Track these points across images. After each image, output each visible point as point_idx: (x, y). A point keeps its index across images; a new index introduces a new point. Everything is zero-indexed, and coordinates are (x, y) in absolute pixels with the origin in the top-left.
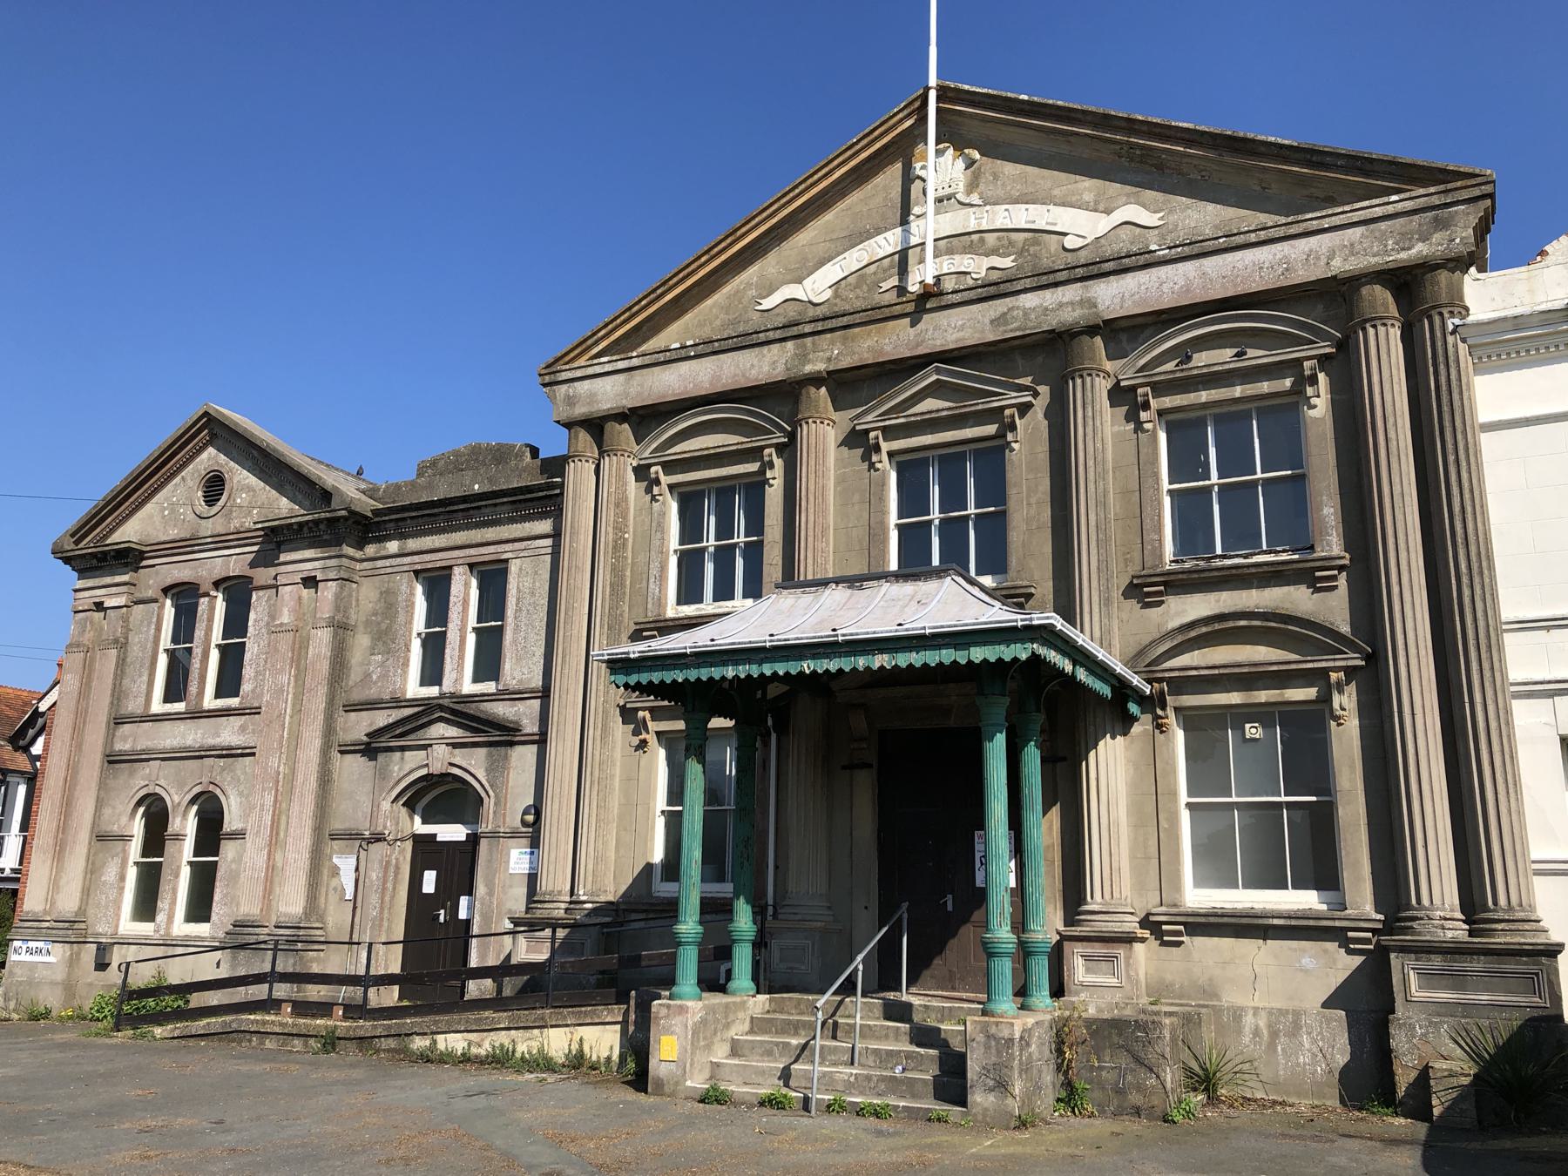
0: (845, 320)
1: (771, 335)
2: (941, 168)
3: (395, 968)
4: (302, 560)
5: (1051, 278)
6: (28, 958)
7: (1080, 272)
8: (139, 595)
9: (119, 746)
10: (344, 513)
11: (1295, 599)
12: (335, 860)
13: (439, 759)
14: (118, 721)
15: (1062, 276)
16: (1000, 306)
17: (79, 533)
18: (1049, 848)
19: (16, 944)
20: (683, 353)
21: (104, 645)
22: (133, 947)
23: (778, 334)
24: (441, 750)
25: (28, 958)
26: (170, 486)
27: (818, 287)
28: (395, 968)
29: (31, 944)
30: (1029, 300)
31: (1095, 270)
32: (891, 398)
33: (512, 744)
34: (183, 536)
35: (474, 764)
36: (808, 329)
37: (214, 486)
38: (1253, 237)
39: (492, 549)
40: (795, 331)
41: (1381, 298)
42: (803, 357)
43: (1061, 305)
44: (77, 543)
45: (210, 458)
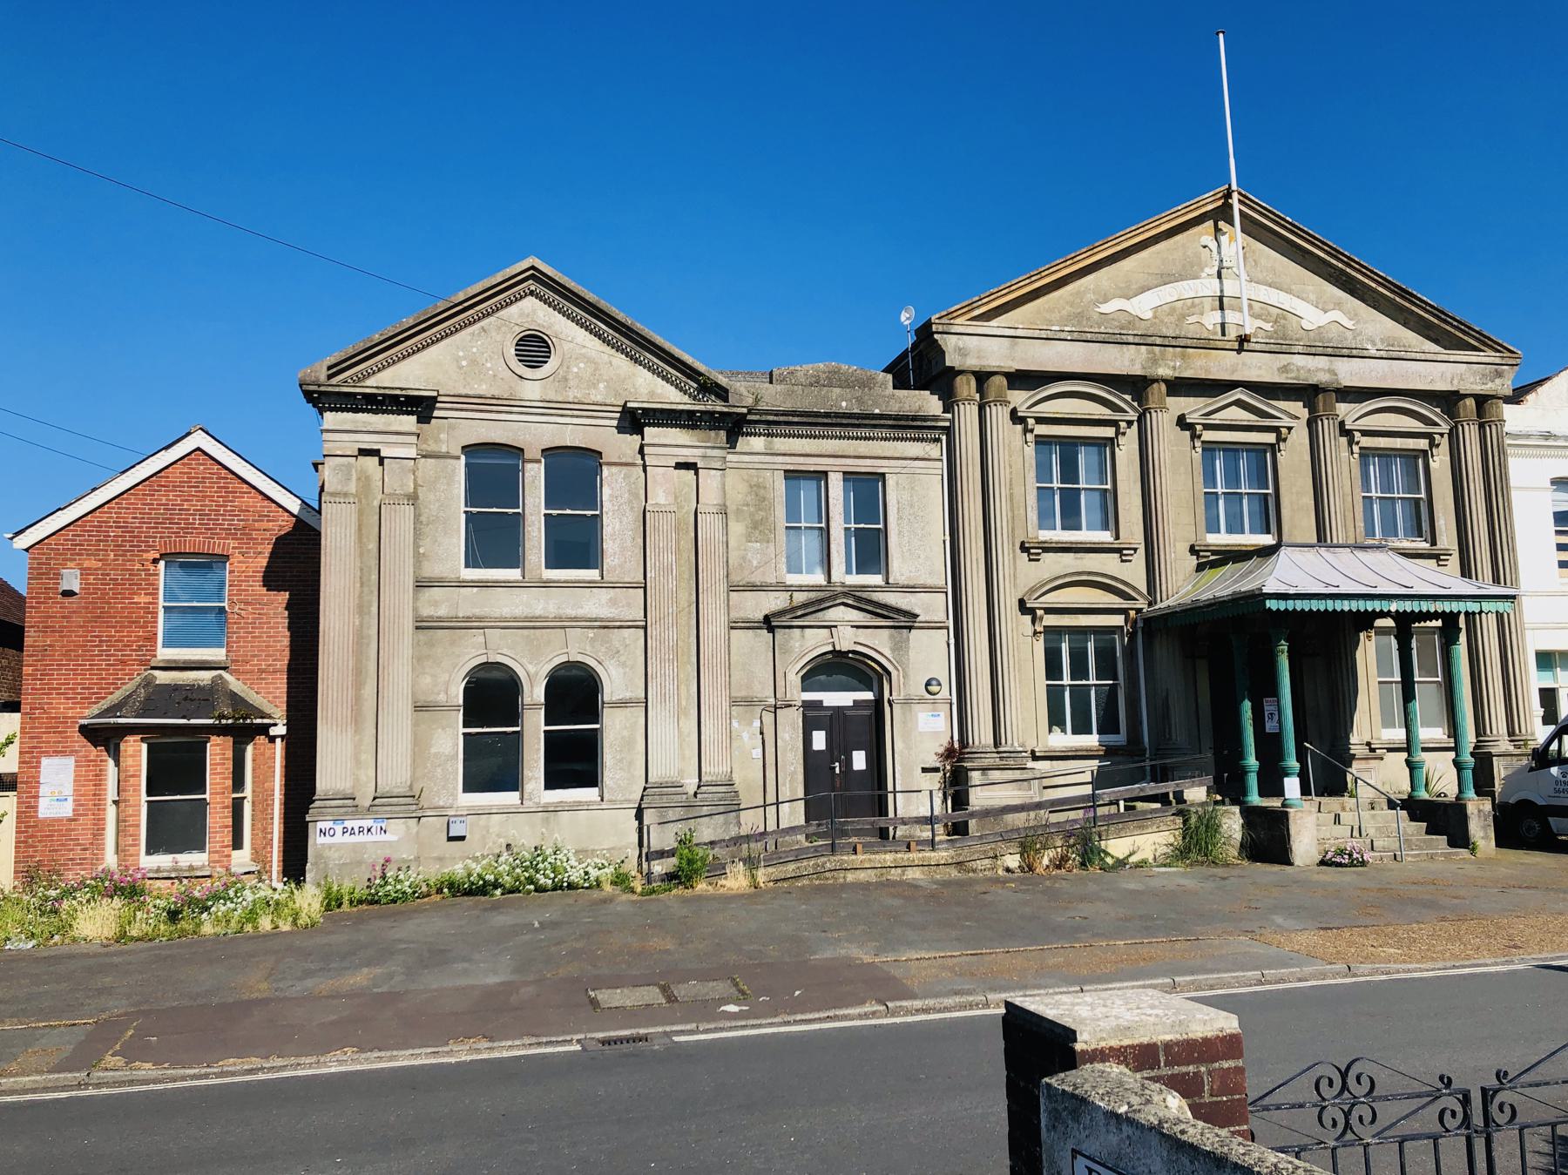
1: (1131, 339)
4: (669, 441)
6: (347, 838)
7: (1330, 351)
8: (432, 447)
9: (426, 612)
11: (1108, 564)
13: (846, 640)
14: (421, 584)
15: (1320, 350)
16: (1284, 359)
18: (793, 774)
21: (395, 500)
23: (1137, 340)
24: (846, 630)
27: (1143, 306)
31: (1337, 352)
33: (910, 628)
34: (496, 393)
35: (878, 643)
36: (1159, 341)
37: (534, 348)
38: (1418, 356)
39: (868, 462)
40: (1149, 340)
41: (1470, 402)
42: (1155, 361)
43: (1318, 370)
45: (532, 313)
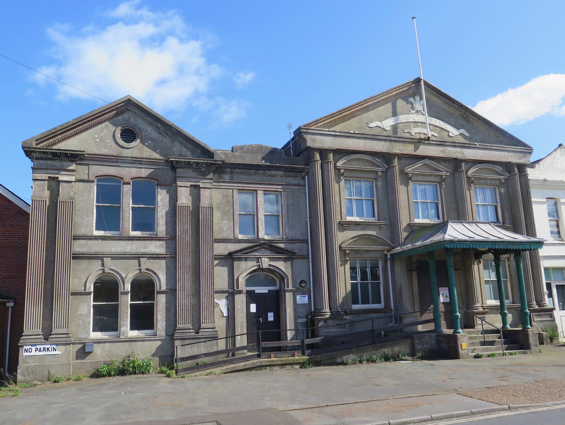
0: (404, 140)
1: (383, 138)
2: (420, 104)
3: (245, 343)
5: (455, 144)
6: (38, 353)
7: (461, 145)
10: (220, 163)
12: (216, 301)
17: (40, 140)
19: (25, 347)
20: (354, 135)
22: (107, 344)
25: (38, 353)
26: (100, 126)
28: (245, 343)
29: (38, 347)
30: (450, 149)
32: (415, 165)
44: (36, 145)
